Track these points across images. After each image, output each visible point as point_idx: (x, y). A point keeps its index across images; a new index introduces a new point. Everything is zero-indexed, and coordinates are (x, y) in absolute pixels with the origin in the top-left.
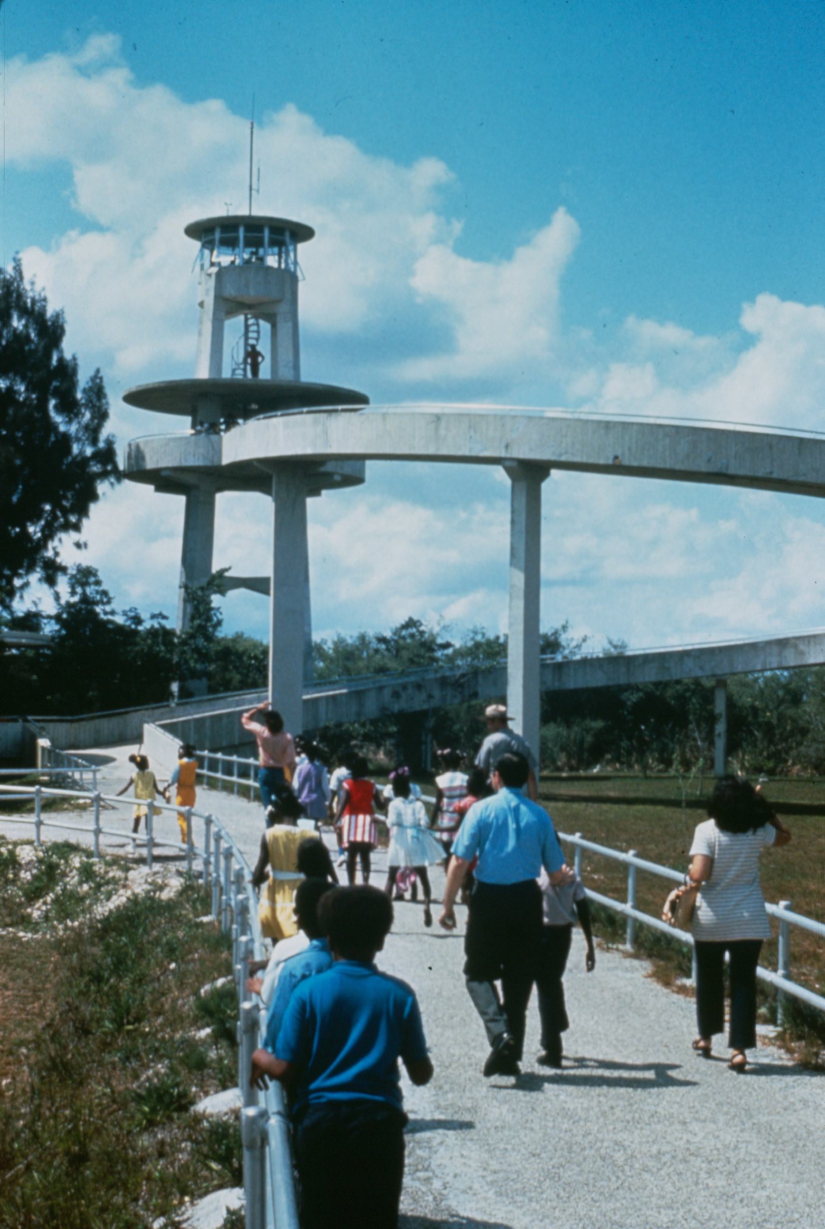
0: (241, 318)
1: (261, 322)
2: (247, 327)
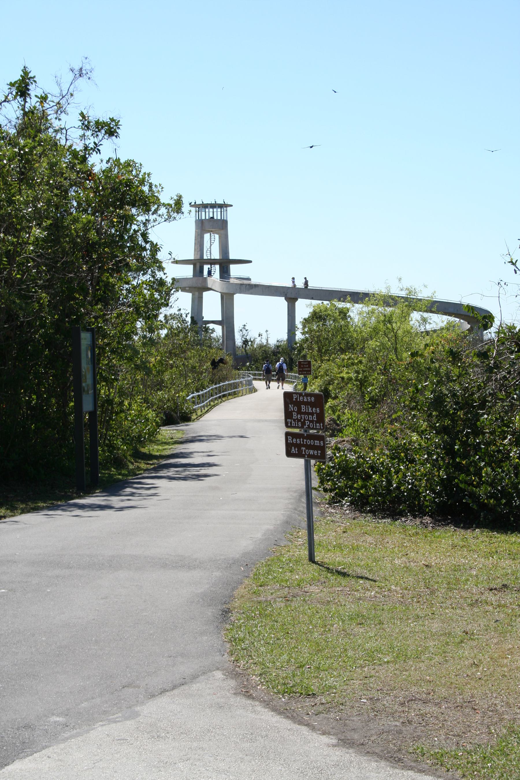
0: (209, 234)
1: (216, 235)
2: (211, 236)
